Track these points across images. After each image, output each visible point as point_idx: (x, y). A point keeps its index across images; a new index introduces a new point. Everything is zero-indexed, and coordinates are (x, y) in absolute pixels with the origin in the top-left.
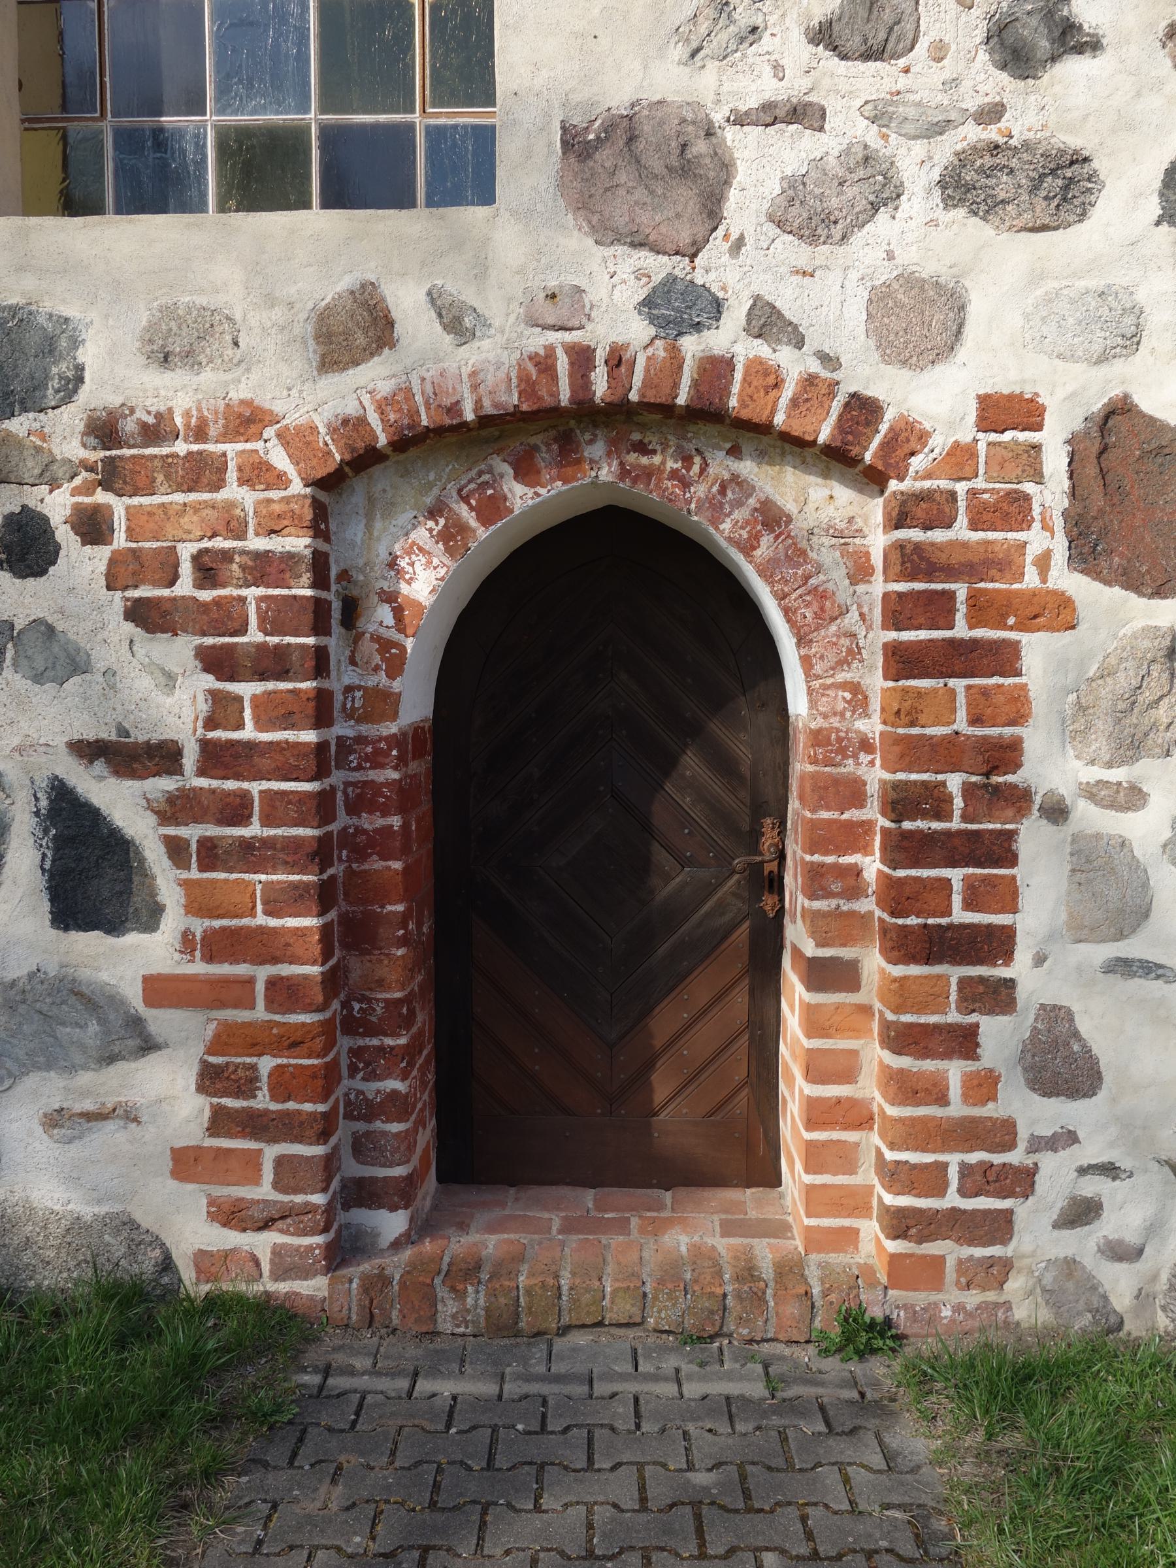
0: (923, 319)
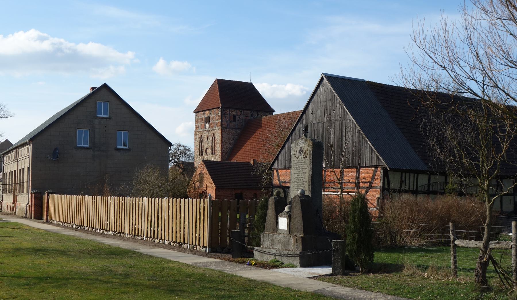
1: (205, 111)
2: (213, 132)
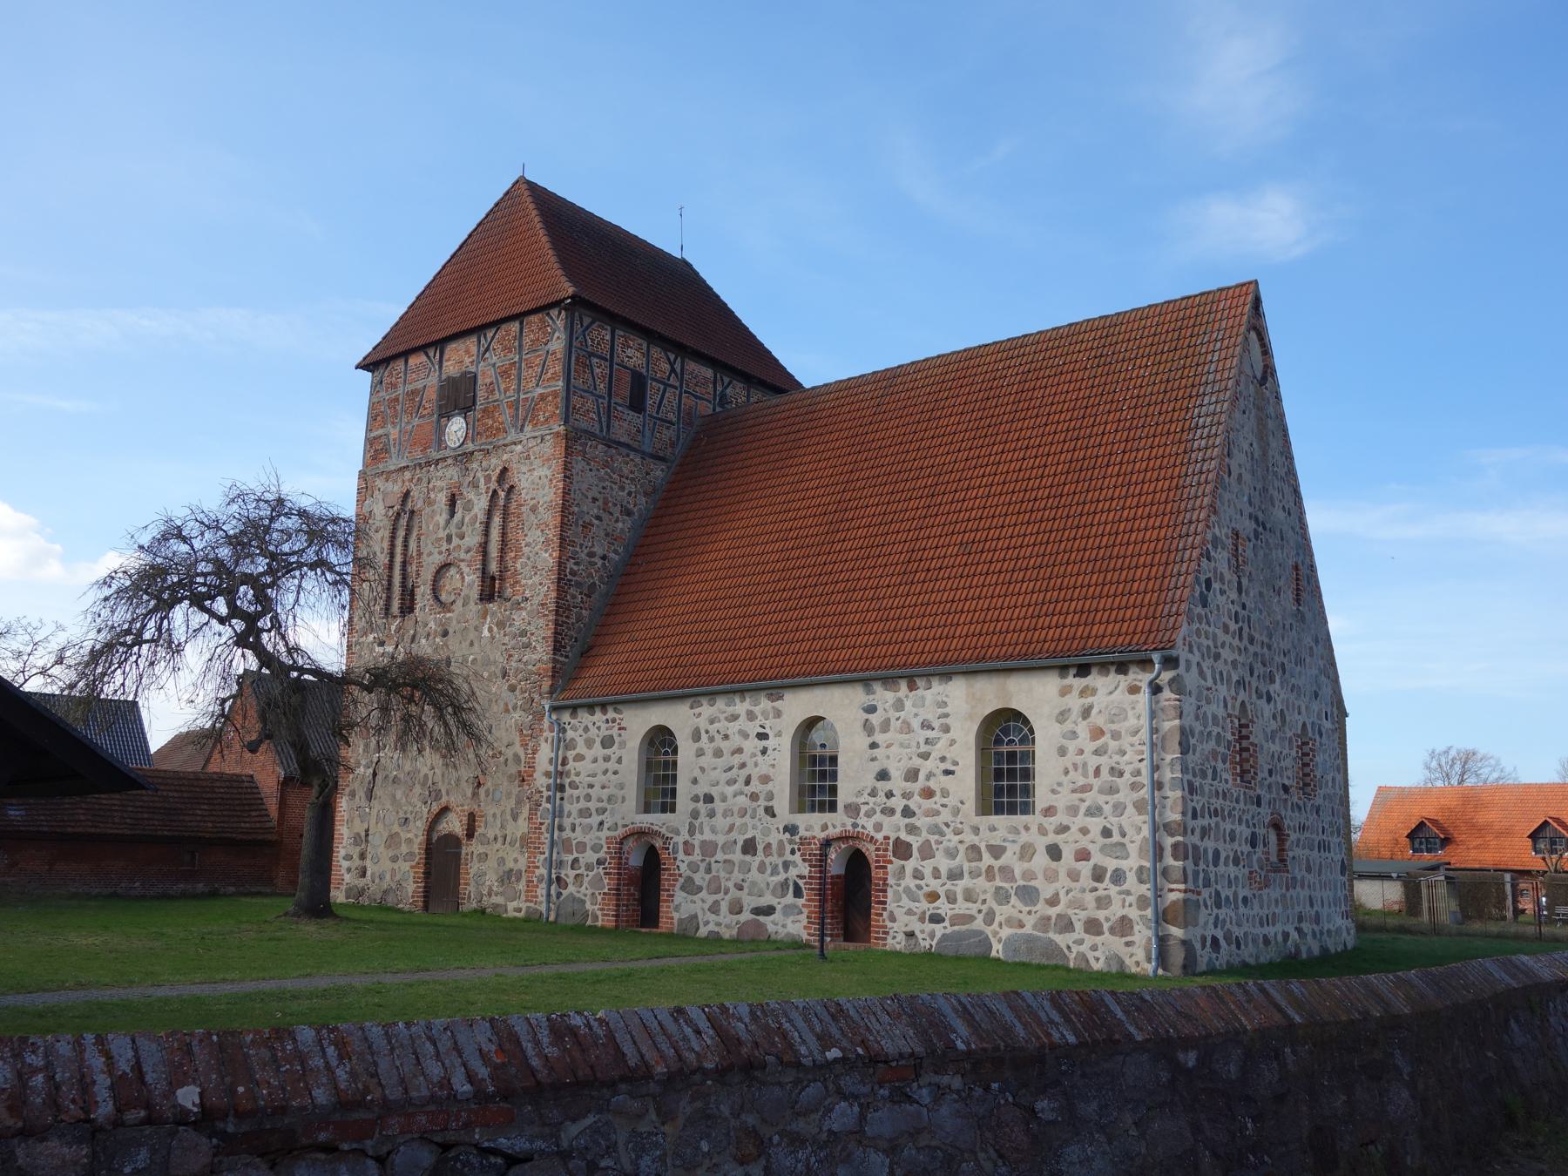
0: (878, 827)
1: (441, 344)
2: (496, 463)
